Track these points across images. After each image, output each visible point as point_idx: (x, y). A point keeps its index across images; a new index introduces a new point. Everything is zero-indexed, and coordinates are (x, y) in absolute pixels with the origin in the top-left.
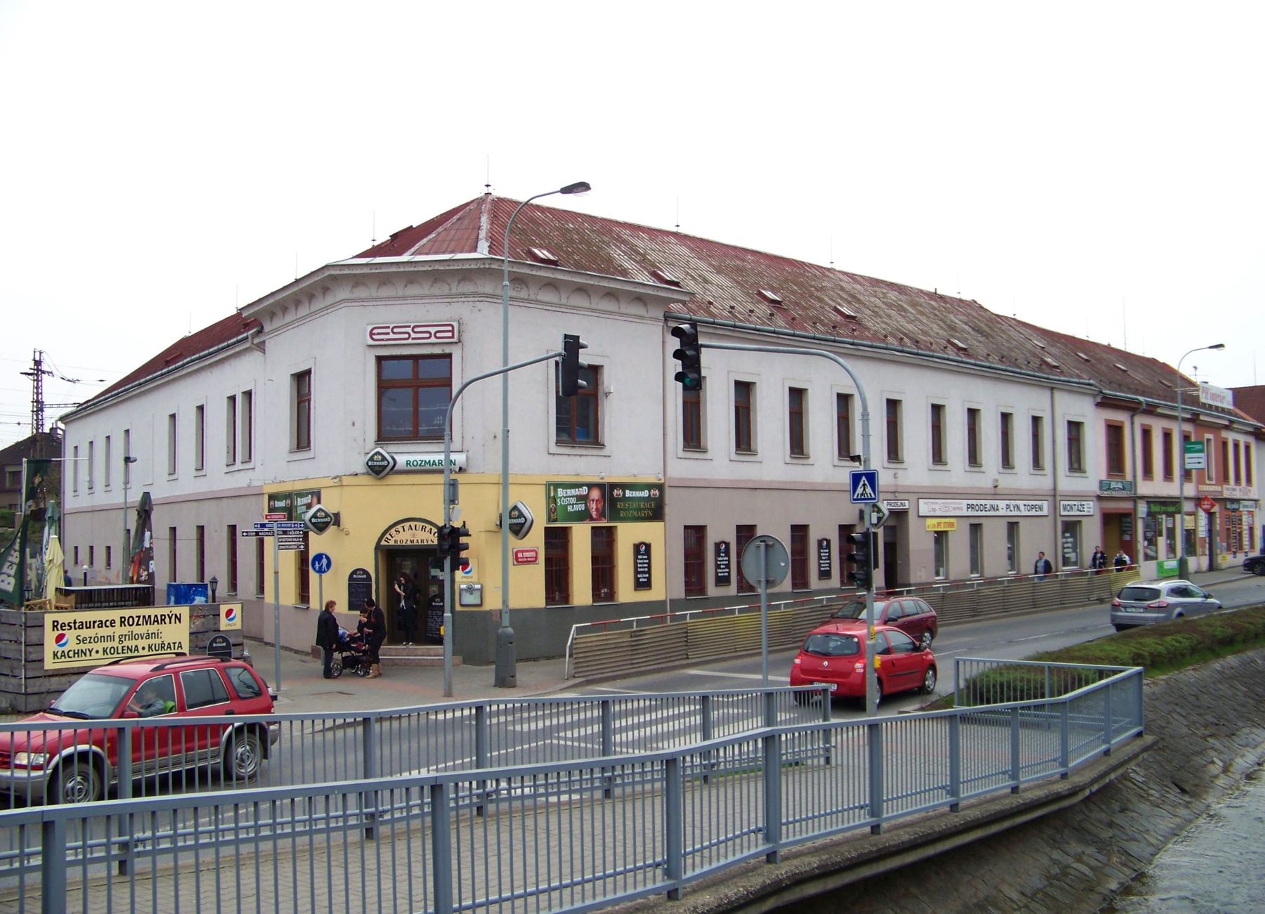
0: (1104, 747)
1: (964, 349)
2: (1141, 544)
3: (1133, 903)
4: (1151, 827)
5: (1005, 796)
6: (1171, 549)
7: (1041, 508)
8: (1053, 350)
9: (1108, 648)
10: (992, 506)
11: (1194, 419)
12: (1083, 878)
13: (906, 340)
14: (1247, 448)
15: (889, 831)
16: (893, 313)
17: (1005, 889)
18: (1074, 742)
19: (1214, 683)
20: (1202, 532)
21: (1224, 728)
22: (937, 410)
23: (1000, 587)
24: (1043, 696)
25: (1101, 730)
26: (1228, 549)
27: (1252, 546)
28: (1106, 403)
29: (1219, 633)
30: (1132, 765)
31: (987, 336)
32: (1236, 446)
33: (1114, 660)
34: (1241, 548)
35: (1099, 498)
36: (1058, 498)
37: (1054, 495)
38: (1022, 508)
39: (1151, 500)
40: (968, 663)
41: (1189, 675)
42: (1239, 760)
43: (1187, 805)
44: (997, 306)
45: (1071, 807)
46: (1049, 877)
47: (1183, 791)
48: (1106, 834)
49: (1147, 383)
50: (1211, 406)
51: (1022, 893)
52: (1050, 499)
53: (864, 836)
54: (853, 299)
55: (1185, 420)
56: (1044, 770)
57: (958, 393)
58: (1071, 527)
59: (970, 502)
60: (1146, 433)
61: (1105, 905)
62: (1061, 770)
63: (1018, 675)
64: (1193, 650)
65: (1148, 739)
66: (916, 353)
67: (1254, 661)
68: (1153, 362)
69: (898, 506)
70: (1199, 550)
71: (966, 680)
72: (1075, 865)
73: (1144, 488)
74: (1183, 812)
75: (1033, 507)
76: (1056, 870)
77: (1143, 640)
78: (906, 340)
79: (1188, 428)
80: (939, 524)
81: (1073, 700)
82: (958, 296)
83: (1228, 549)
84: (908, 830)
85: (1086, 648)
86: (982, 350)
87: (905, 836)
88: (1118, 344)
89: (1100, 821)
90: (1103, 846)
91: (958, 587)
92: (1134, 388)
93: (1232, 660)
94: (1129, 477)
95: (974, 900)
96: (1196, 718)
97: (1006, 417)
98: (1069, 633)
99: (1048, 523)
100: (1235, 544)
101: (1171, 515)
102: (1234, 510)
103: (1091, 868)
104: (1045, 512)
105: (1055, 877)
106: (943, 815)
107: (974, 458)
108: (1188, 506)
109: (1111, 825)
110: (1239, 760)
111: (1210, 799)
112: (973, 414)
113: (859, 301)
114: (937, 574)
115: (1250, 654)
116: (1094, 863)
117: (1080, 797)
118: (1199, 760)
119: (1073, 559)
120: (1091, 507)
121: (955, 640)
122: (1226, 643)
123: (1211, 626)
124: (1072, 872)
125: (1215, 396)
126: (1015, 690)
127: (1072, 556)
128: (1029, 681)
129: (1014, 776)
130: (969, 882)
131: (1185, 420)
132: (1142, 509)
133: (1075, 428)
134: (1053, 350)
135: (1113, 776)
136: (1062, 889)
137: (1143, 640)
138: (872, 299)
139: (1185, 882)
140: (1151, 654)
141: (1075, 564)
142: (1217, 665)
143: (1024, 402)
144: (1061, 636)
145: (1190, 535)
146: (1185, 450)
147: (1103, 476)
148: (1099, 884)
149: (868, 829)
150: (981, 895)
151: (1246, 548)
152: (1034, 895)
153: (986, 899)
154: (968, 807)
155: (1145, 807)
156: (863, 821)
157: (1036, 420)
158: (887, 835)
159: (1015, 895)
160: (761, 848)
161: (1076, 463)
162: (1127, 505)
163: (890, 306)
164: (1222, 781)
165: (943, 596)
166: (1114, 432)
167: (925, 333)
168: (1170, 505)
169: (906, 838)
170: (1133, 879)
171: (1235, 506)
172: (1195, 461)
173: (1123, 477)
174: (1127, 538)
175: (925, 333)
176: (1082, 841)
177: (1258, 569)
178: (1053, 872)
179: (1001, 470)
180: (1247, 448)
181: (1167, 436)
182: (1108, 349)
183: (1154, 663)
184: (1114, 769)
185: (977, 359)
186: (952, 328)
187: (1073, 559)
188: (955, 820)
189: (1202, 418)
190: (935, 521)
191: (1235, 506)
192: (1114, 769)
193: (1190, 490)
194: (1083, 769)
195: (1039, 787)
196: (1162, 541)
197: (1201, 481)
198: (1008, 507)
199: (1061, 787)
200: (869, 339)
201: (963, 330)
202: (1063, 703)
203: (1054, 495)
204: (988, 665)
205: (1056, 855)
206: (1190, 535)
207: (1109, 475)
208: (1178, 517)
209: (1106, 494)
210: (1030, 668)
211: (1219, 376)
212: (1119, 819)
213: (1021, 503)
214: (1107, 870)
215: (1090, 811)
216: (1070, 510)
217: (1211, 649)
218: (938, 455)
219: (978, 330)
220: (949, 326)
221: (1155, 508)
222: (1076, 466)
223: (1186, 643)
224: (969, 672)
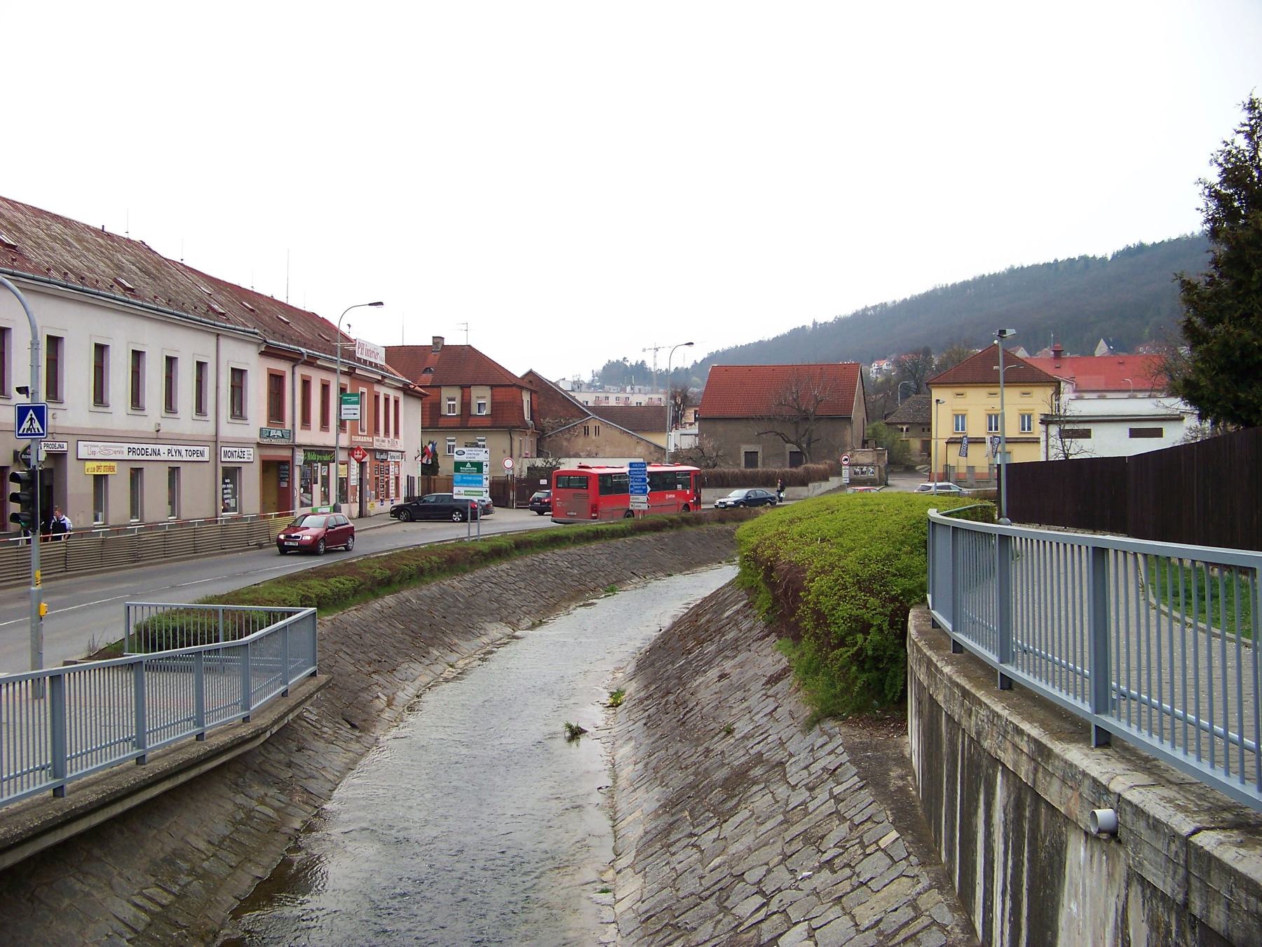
0: (282, 688)
1: (132, 290)
2: (298, 491)
3: (317, 840)
4: (327, 764)
5: (190, 744)
6: (326, 496)
7: (202, 455)
8: (220, 298)
9: (274, 590)
10: (153, 450)
11: (350, 373)
12: (268, 820)
13: (70, 275)
14: (396, 402)
15: (153, 760)
16: (57, 246)
17: (191, 839)
18: (256, 684)
19: (375, 622)
20: (354, 481)
21: (385, 664)
22: (101, 350)
23: (161, 532)
24: (217, 640)
25: (273, 671)
26: (377, 497)
27: (397, 495)
28: (269, 352)
29: (378, 574)
30: (307, 705)
31: (154, 278)
32: (387, 400)
33: (284, 602)
34: (388, 496)
35: (259, 445)
36: (219, 445)
37: (216, 441)
38: (184, 453)
39: (308, 449)
40: (139, 608)
41: (353, 615)
42: (400, 693)
43: (358, 739)
44: (167, 249)
45: (250, 751)
46: (235, 823)
47: (353, 726)
48: (286, 774)
49: (309, 336)
50: (365, 361)
51: (210, 842)
52: (212, 445)
53: (46, 801)
54: (14, 227)
55: (343, 373)
56: (225, 715)
57: (123, 334)
58: (231, 474)
59: (132, 446)
60: (306, 383)
61: (291, 844)
62: (197, 730)
63: (191, 619)
64: (356, 591)
65: (322, 678)
66: (82, 290)
67: (408, 600)
68: (313, 316)
69: (56, 448)
70: (351, 498)
71: (137, 627)
72: (258, 808)
73: (303, 437)
74: (355, 746)
75: (194, 452)
76: (241, 815)
77: (308, 583)
78: (70, 275)
79: (345, 380)
80: (99, 467)
81: (254, 642)
82: (126, 236)
83: (377, 497)
84: (94, 788)
85: (255, 591)
86: (149, 292)
87: (92, 796)
88: (280, 297)
89: (279, 762)
90: (284, 786)
91: (118, 532)
92: (296, 340)
93: (389, 600)
94: (288, 426)
95: (162, 855)
96: (361, 656)
97: (171, 361)
98: (233, 577)
99: (209, 468)
100: (383, 495)
101: (326, 463)
102: (383, 461)
103: (277, 810)
104: (206, 458)
105: (241, 822)
106: (129, 769)
107: (136, 401)
108: (342, 456)
109: (290, 765)
110: (400, 693)
111: (378, 732)
112: (137, 355)
113: (20, 230)
114: (96, 519)
115: (406, 593)
116: (277, 804)
117: (262, 739)
118: (365, 696)
119: (233, 505)
120: (251, 454)
121: (117, 587)
122: (386, 584)
123: (370, 568)
124: (257, 815)
125: (370, 352)
126: (188, 635)
127: (232, 503)
128: (202, 625)
129: (199, 723)
130: (154, 837)
131: (343, 373)
132: (300, 457)
133: (238, 375)
134: (220, 298)
135: (291, 717)
136: (249, 833)
137: (308, 583)
138: (35, 230)
139: (362, 814)
140: (317, 596)
141: (234, 509)
142: (376, 605)
143: (190, 347)
144: (222, 580)
145: (343, 482)
146: (341, 402)
147: (264, 424)
148: (283, 825)
149: (50, 793)
150: (168, 849)
151: (392, 496)
152: (221, 843)
153: (174, 852)
154: (157, 757)
155: (320, 745)
156: (44, 784)
157: (201, 366)
158: (71, 797)
159: (202, 845)
160: (50, 782)
161: (238, 411)
162: (286, 453)
163: (54, 239)
164: (387, 715)
165: (103, 541)
166: (276, 381)
167: (91, 270)
168: (325, 454)
169: (93, 798)
170: (315, 816)
171: (383, 457)
172: (351, 412)
173: (283, 425)
174: (285, 485)
175: (91, 270)
176: (264, 783)
177: (403, 516)
178: (238, 818)
179: (164, 414)
180: (396, 402)
181: (325, 388)
182: (271, 300)
183: (323, 603)
184: (292, 710)
185: (143, 300)
186: (119, 267)
187: (233, 505)
188: (144, 773)
189: (357, 371)
190: (95, 464)
191: (383, 457)
192: (292, 710)
193: (344, 440)
194: (263, 711)
195: (221, 732)
196: (317, 489)
197: (354, 432)
198: (169, 451)
199: (245, 731)
200: (30, 270)
201: (131, 271)
202: (246, 646)
203: (216, 441)
204: (160, 610)
205: (240, 799)
206: (343, 482)
207: (269, 423)
208: (332, 466)
209: (266, 441)
210: (202, 612)
211: (375, 334)
212: (298, 759)
213: (183, 448)
214: (290, 809)
215: (269, 752)
216: (230, 457)
217: (371, 590)
218: (100, 397)
219: (147, 273)
220: (116, 265)
221: (312, 457)
222: (238, 413)
223: (349, 585)
224: (140, 617)
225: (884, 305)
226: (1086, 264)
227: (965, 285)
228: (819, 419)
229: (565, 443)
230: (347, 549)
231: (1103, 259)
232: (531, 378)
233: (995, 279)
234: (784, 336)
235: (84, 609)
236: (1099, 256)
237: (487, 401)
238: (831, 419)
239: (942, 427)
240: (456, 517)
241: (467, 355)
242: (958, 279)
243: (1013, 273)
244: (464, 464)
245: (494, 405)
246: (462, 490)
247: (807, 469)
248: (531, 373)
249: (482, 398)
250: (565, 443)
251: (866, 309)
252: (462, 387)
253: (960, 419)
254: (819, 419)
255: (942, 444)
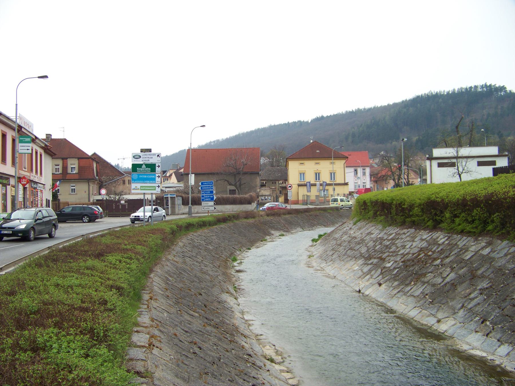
14: (41, 155)
32: (36, 153)
102: (35, 188)
108: (12, 181)
145: (14, 199)
171: (35, 186)
191: (35, 186)
208: (9, 187)
225: (218, 141)
226: (301, 124)
227: (252, 132)
228: (245, 173)
229: (113, 189)
230: (51, 236)
231: (307, 122)
232: (95, 157)
233: (264, 130)
234: (176, 153)
235: (80, 204)
236: (305, 120)
237: (76, 166)
238: (252, 173)
239: (293, 178)
240: (86, 219)
241: (64, 143)
242: (249, 130)
243: (271, 127)
244: (140, 166)
245: (80, 167)
246: (139, 185)
247: (251, 196)
248: (95, 154)
249: (73, 165)
250: (113, 189)
251: (211, 142)
252: (63, 159)
253: (302, 175)
254: (245, 173)
255: (295, 187)
